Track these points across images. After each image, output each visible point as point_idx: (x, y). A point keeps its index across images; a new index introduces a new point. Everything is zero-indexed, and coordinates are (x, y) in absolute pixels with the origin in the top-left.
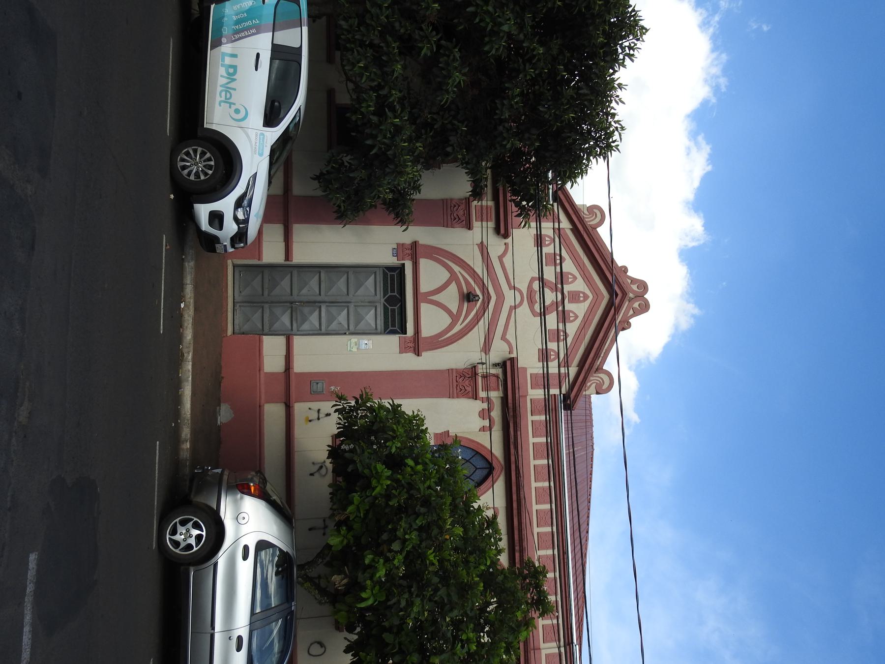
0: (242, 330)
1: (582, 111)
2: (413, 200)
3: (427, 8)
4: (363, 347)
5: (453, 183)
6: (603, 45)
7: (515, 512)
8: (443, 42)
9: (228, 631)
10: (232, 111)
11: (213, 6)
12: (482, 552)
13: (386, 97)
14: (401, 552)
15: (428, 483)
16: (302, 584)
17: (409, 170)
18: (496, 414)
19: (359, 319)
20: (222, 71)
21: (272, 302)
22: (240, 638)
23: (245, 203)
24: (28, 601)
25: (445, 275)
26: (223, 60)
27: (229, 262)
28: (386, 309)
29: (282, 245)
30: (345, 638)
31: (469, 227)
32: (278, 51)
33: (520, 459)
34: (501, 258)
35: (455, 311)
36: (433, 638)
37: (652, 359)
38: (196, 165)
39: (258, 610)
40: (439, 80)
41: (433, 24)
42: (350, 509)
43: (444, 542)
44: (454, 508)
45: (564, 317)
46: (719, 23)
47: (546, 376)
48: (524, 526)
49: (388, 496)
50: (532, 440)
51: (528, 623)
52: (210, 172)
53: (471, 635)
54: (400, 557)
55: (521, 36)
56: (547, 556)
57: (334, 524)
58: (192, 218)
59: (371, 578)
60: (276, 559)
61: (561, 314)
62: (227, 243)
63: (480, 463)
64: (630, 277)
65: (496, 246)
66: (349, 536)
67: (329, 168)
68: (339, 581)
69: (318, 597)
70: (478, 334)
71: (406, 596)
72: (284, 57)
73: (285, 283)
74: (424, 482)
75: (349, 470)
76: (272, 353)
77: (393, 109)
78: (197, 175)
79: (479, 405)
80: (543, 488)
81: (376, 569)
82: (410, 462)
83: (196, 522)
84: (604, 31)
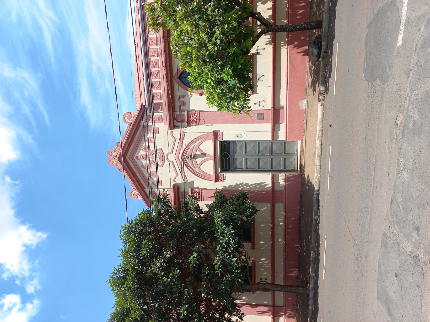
18: (177, 104)
24: (404, 20)
28: (229, 152)
70: (186, 142)
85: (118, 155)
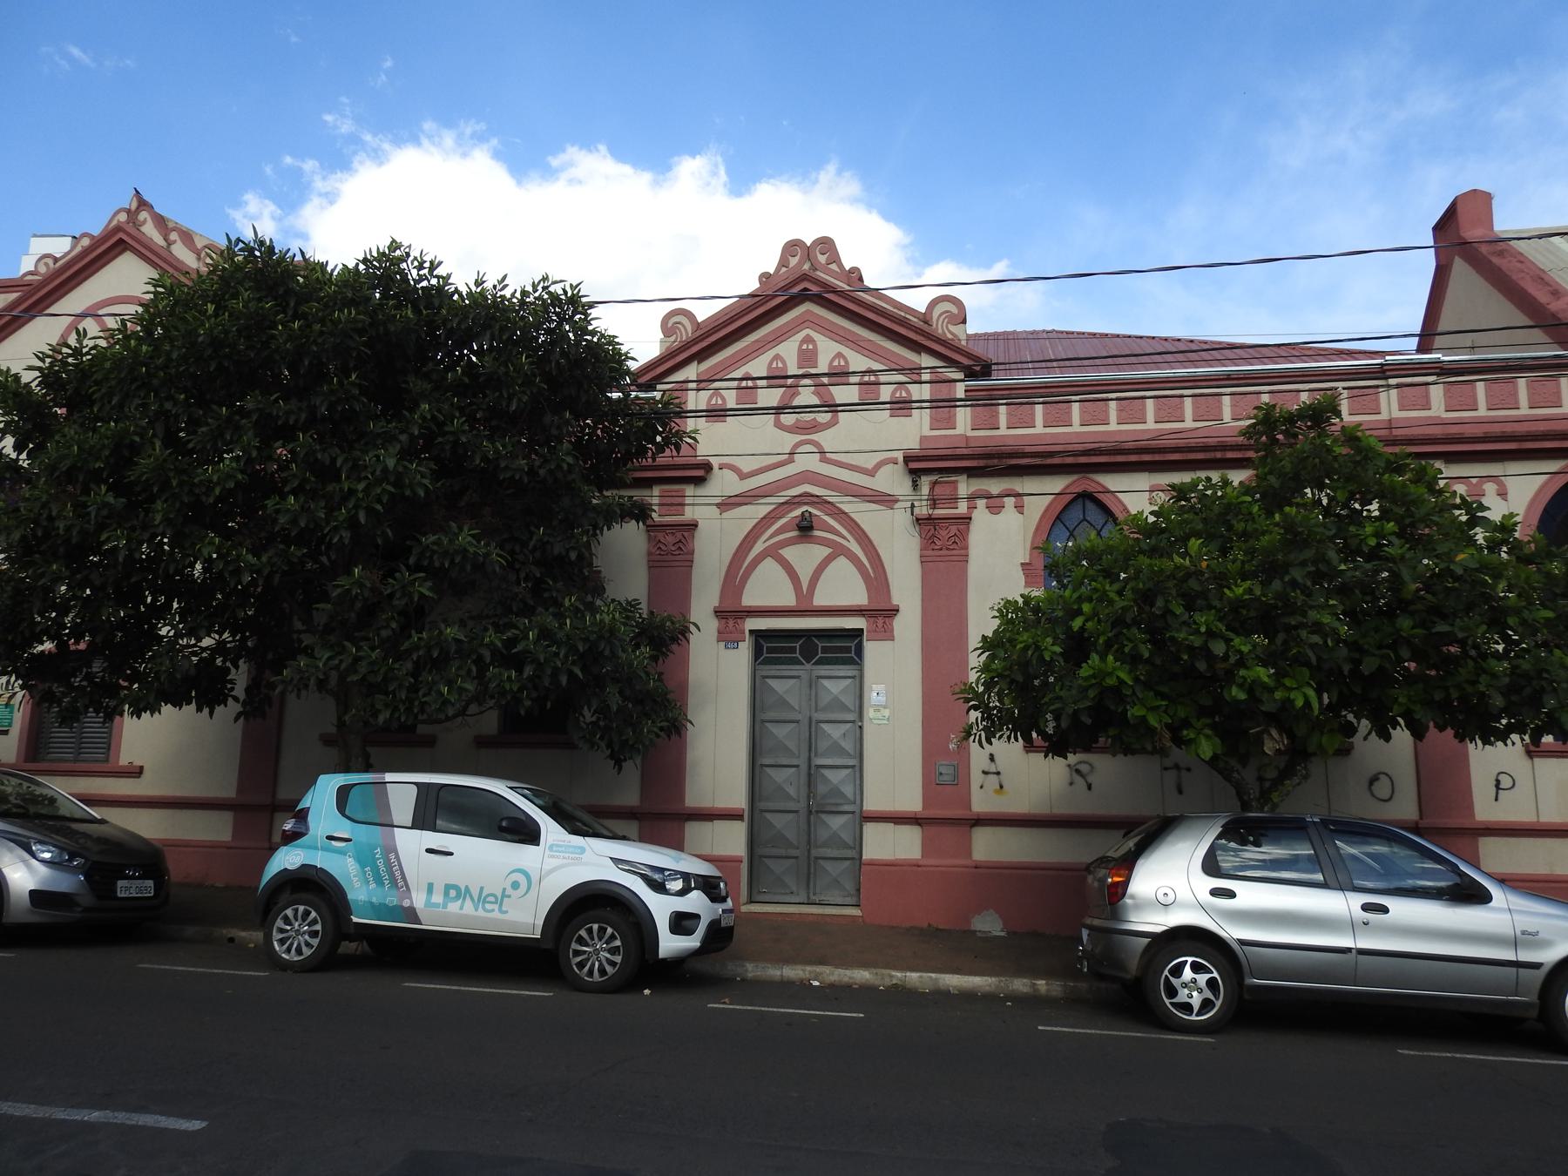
0: (853, 892)
1: (516, 343)
2: (652, 613)
3: (361, 586)
4: (882, 699)
5: (624, 553)
6: (416, 310)
7: (1157, 457)
8: (412, 561)
9: (1353, 927)
10: (515, 894)
11: (355, 920)
12: (1230, 509)
13: (495, 652)
14: (1228, 641)
15: (1112, 595)
16: (1275, 806)
17: (607, 619)
18: (995, 486)
19: (837, 704)
20: (454, 907)
21: (809, 842)
22: (1366, 908)
23: (657, 877)
25: (769, 565)
26: (437, 905)
27: (744, 909)
28: (821, 662)
29: (719, 825)
30: (1365, 739)
31: (693, 526)
32: (422, 821)
33: (1070, 448)
34: (743, 476)
35: (828, 551)
36: (1372, 592)
37: (907, 240)
38: (598, 952)
39: (1319, 877)
40: (469, 568)
41: (385, 577)
42: (1153, 721)
43: (1213, 571)
44: (1153, 552)
45: (840, 375)
46: (375, 135)
47: (935, 403)
48: (1182, 443)
49: (1134, 660)
50: (1039, 429)
51: (1351, 437)
52: (610, 930)
53: (1369, 529)
54: (1237, 641)
55: (403, 437)
56: (1233, 406)
57: (1175, 749)
58: (678, 962)
59: (1271, 691)
60: (1233, 845)
61: (835, 380)
62: (719, 908)
63: (1075, 514)
64: (778, 269)
65: (723, 483)
66: (1199, 725)
67: (603, 744)
68: (1273, 743)
69: (1296, 780)
70: (867, 515)
71: (1303, 634)
72: (434, 811)
73: (778, 821)
74: (1111, 602)
75: (1089, 721)
76: (888, 845)
77: (512, 642)
78: (613, 951)
79: (981, 514)
80: (1120, 411)
81: (1257, 682)
82: (1077, 623)
83: (1171, 972)
84: (396, 307)
85: (821, 275)
